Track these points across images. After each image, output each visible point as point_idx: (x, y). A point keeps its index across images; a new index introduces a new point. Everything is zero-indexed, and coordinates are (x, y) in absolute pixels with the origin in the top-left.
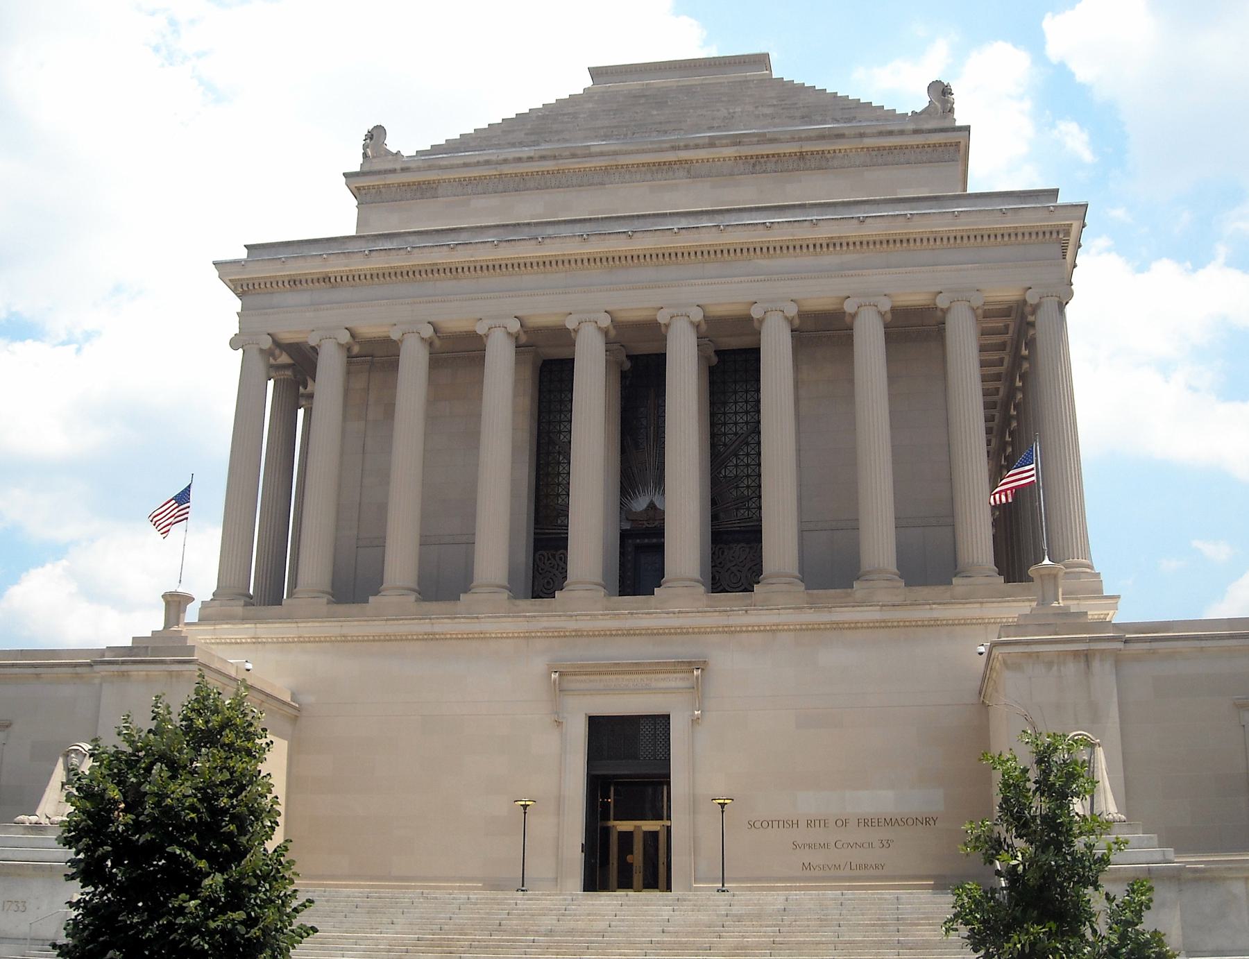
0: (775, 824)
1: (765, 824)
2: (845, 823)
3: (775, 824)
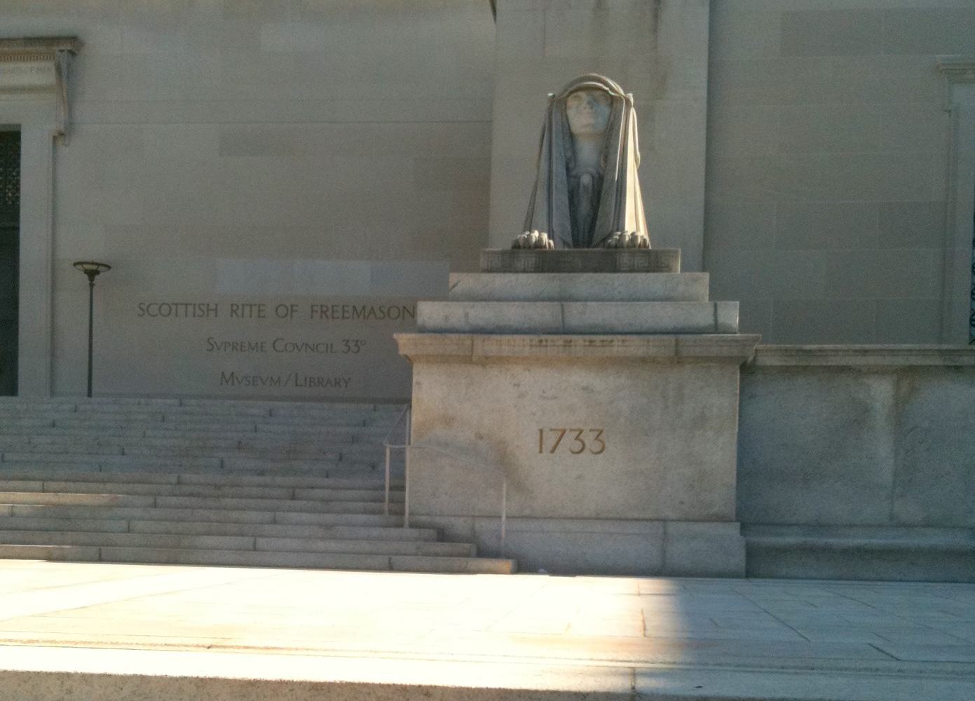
0: (182, 309)
1: (165, 309)
2: (292, 310)
3: (182, 309)
